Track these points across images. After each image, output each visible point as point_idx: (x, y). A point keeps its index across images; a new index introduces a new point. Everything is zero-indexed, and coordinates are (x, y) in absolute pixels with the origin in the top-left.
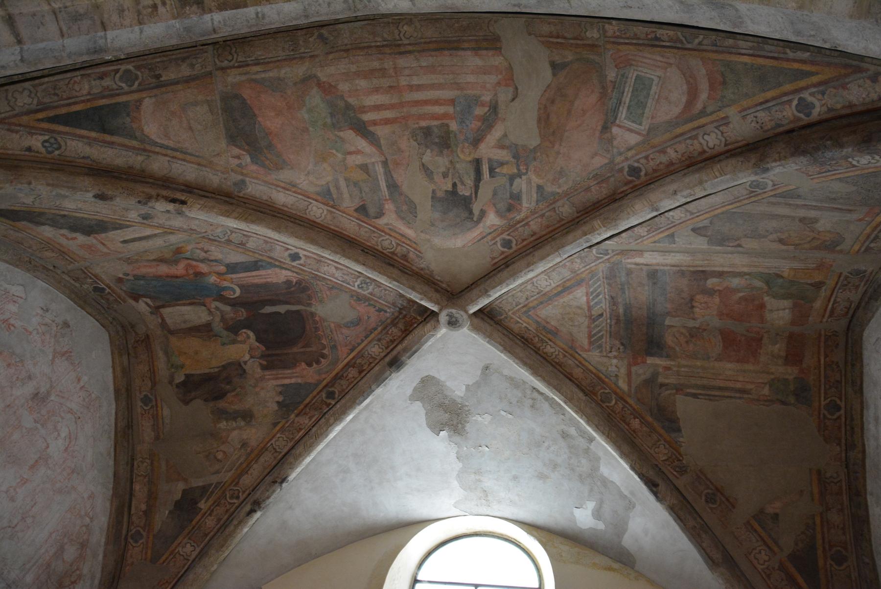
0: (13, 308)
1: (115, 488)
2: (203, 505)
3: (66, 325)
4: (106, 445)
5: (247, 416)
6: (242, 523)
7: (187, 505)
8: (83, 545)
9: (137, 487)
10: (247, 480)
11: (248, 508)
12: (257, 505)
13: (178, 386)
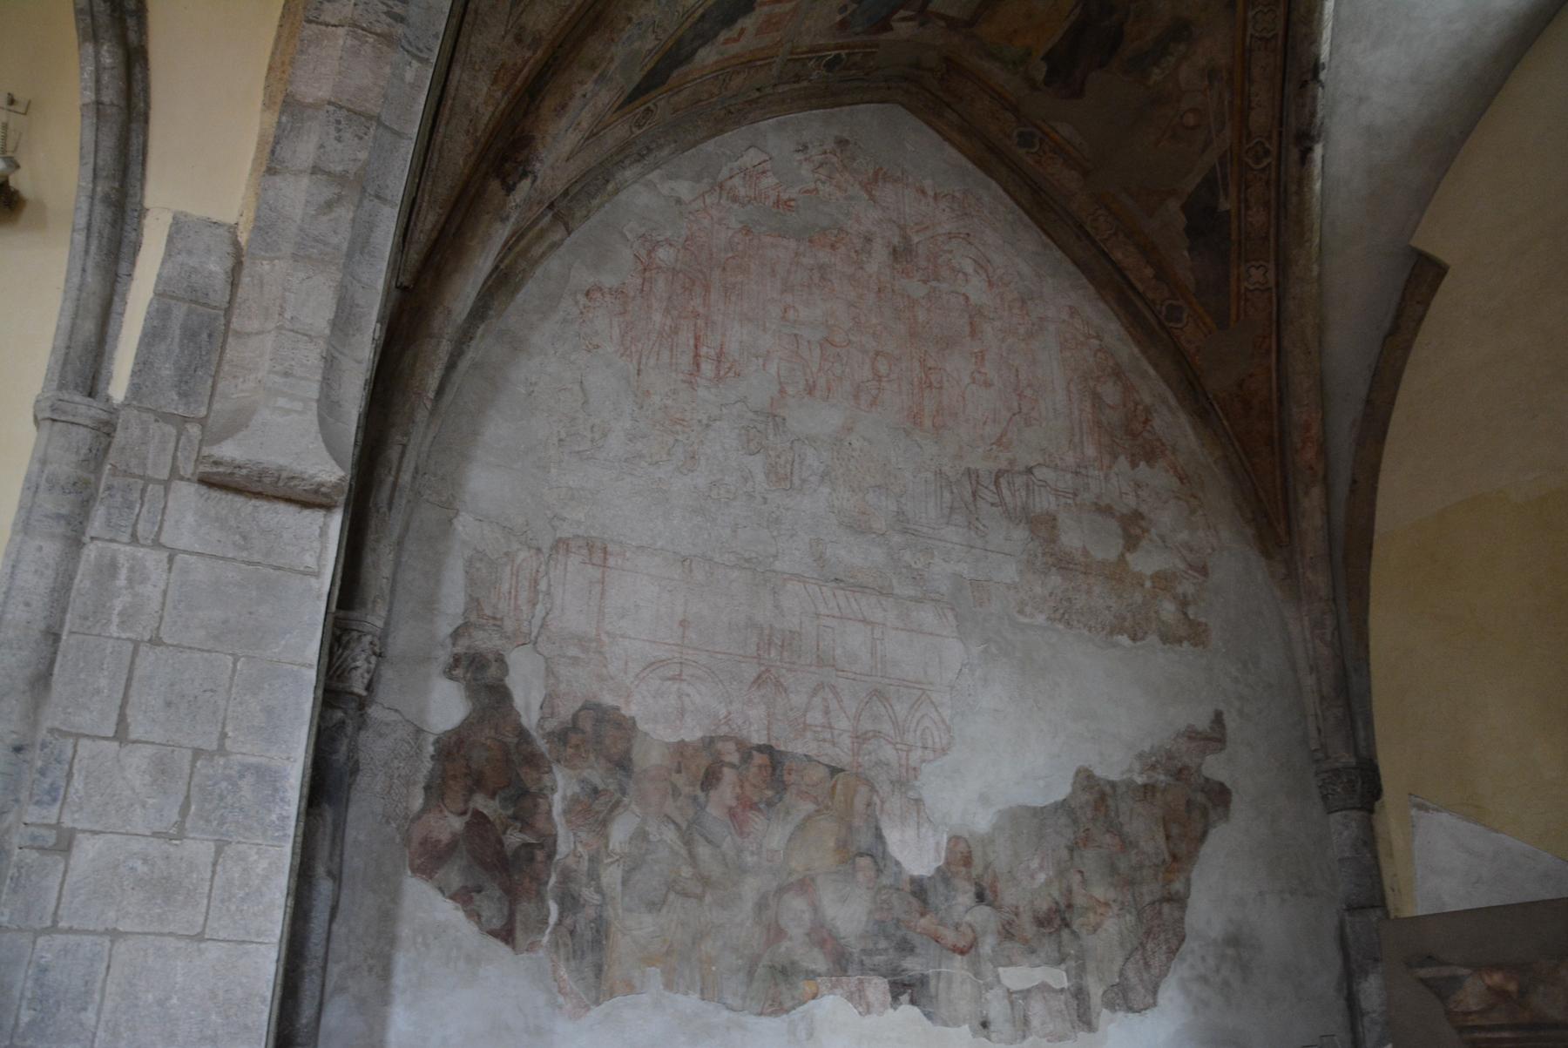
0: (769, 181)
1: (1092, 280)
2: (1226, 205)
3: (842, 143)
4: (1031, 239)
5: (1180, 31)
6: (1303, 181)
7: (1204, 223)
8: (1118, 373)
9: (1118, 255)
10: (1259, 119)
11: (1295, 154)
12: (1305, 140)
13: (1489, 988)
